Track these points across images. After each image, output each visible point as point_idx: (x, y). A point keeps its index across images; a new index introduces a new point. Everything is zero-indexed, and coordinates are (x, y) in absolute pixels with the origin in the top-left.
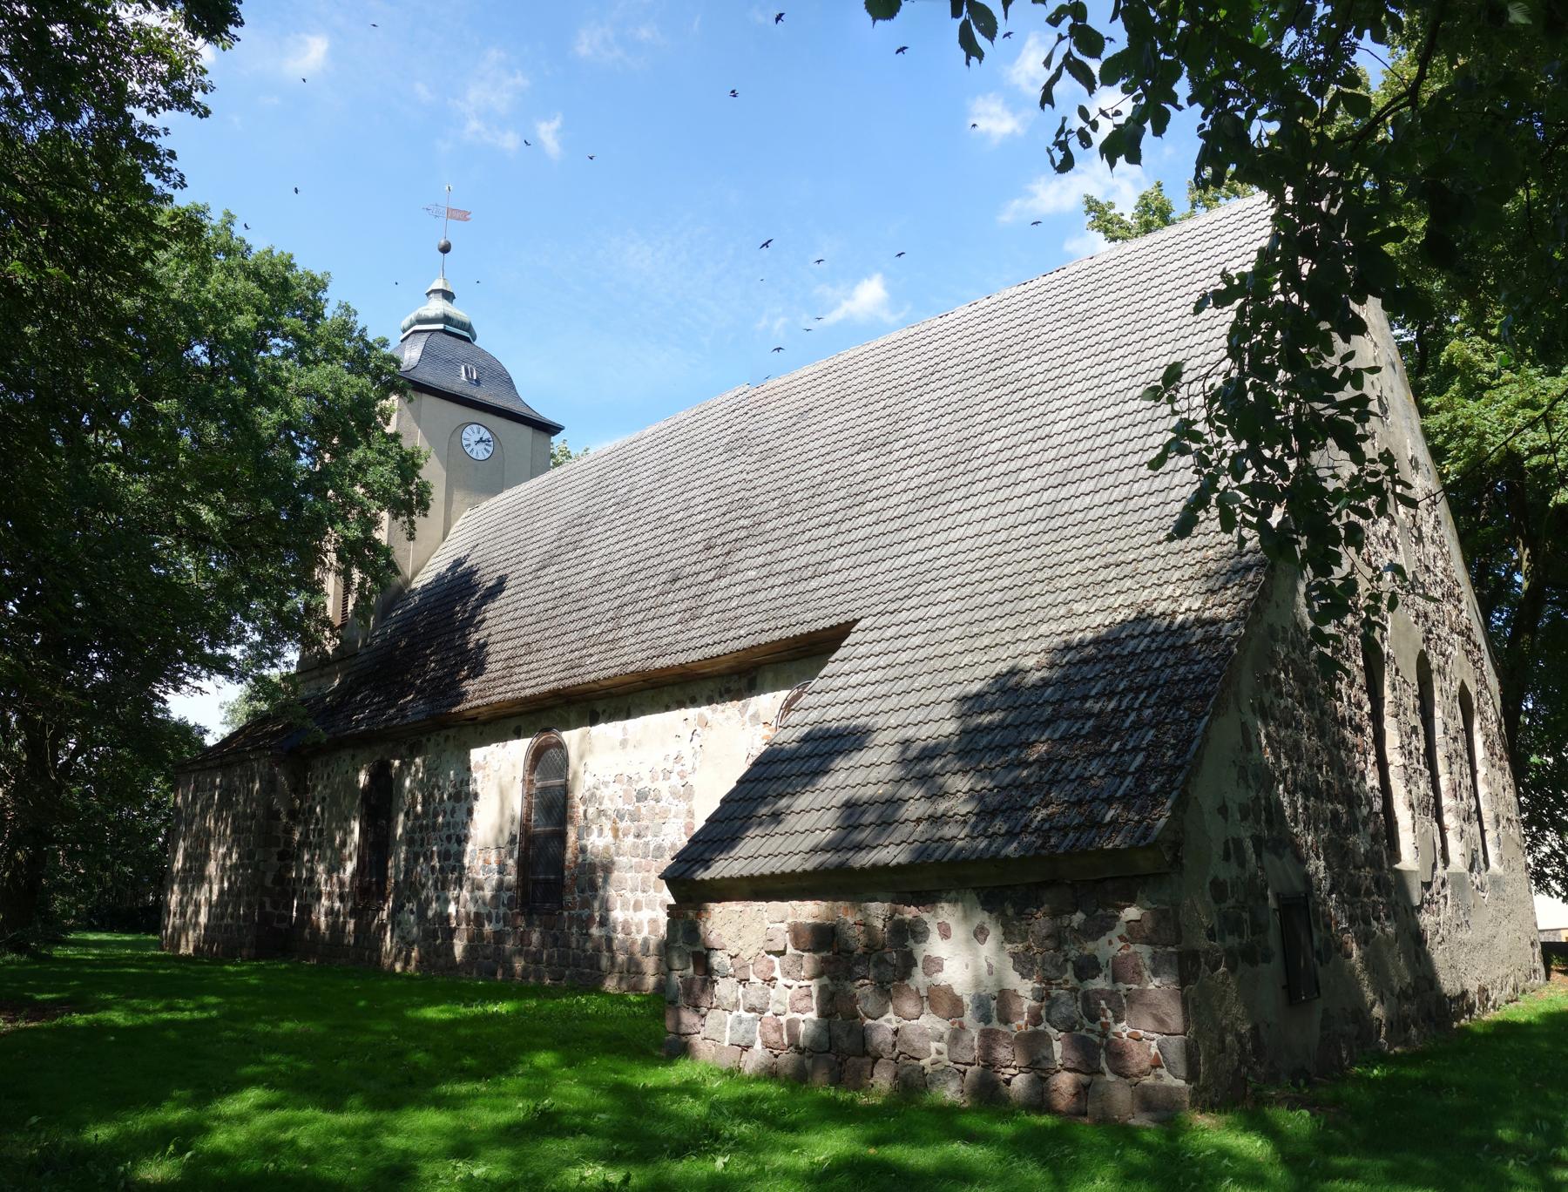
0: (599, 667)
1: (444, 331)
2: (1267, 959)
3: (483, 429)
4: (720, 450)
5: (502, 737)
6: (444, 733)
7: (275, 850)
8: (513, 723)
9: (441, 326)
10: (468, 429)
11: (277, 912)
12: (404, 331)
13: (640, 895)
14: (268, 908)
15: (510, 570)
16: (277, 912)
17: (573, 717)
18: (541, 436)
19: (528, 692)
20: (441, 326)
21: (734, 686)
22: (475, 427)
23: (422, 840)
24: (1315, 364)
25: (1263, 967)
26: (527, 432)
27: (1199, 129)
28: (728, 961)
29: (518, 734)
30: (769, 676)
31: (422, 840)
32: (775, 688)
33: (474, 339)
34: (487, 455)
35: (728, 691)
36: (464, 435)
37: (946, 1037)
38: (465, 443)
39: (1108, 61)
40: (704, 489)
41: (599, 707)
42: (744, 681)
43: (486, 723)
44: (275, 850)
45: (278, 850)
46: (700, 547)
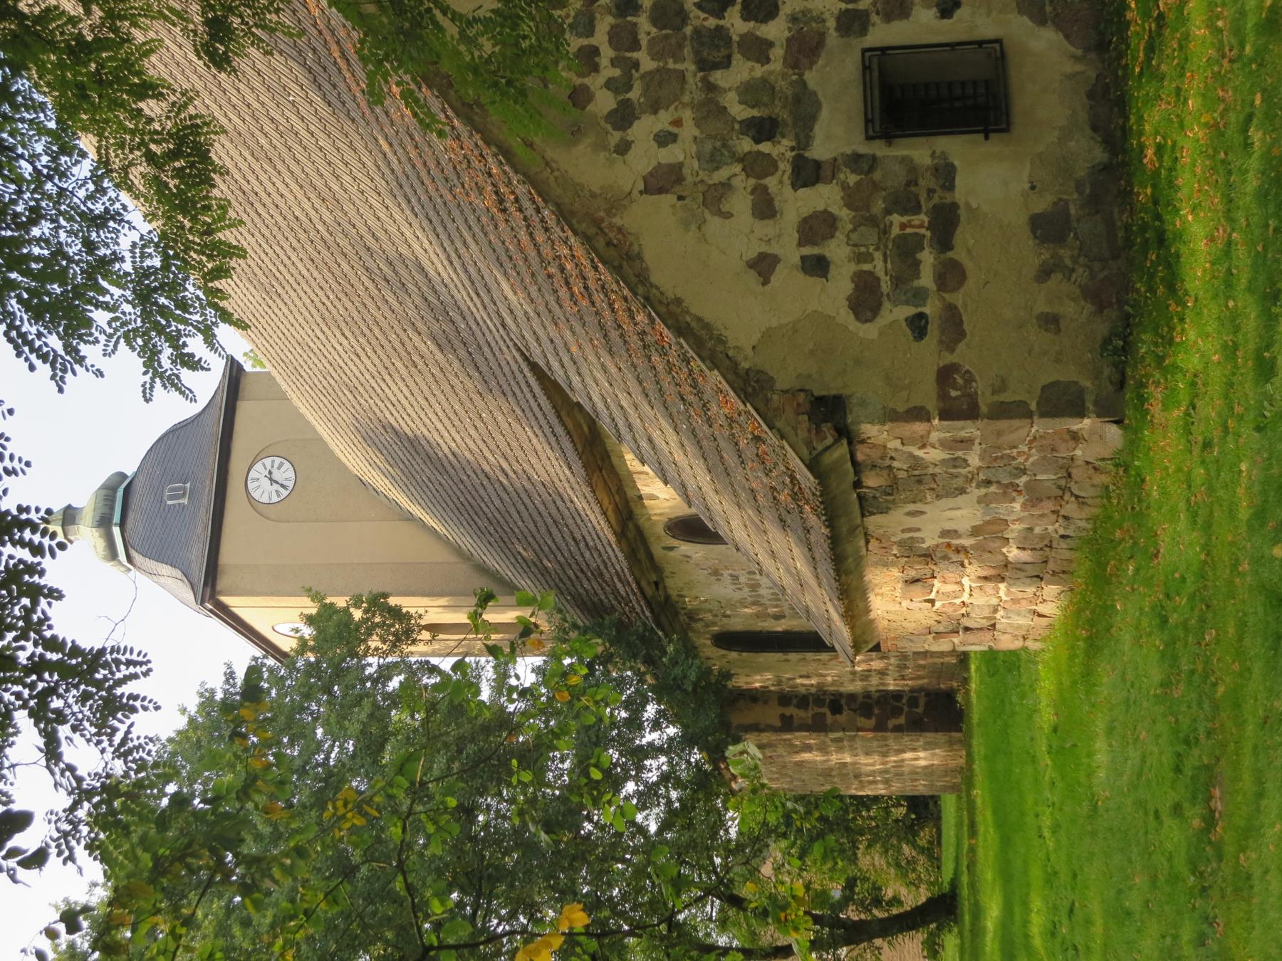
1: (122, 525)
3: (253, 474)
7: (830, 718)
10: (256, 495)
11: (906, 709)
14: (901, 720)
15: (237, 177)
16: (906, 709)
18: (247, 387)
20: (116, 531)
22: (251, 486)
26: (245, 410)
27: (150, 670)
33: (122, 476)
34: (287, 465)
36: (265, 499)
38: (275, 499)
39: (759, 153)
44: (830, 718)
45: (829, 713)
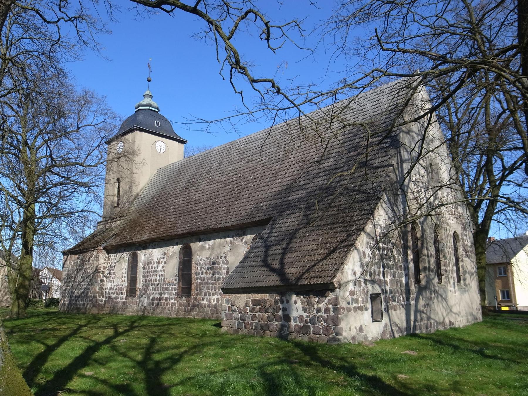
0: (201, 225)
2: (366, 309)
4: (237, 158)
5: (172, 245)
6: (154, 243)
8: (176, 241)
9: (148, 108)
12: (136, 108)
13: (213, 291)
17: (194, 240)
19: (181, 232)
21: (240, 233)
23: (146, 282)
24: (175, 303)
25: (365, 312)
28: (236, 308)
29: (177, 244)
30: (249, 231)
31: (146, 282)
32: (250, 234)
35: (238, 234)
37: (452, 326)
40: (232, 171)
41: (202, 237)
42: (242, 232)
43: (167, 241)
46: (231, 190)
